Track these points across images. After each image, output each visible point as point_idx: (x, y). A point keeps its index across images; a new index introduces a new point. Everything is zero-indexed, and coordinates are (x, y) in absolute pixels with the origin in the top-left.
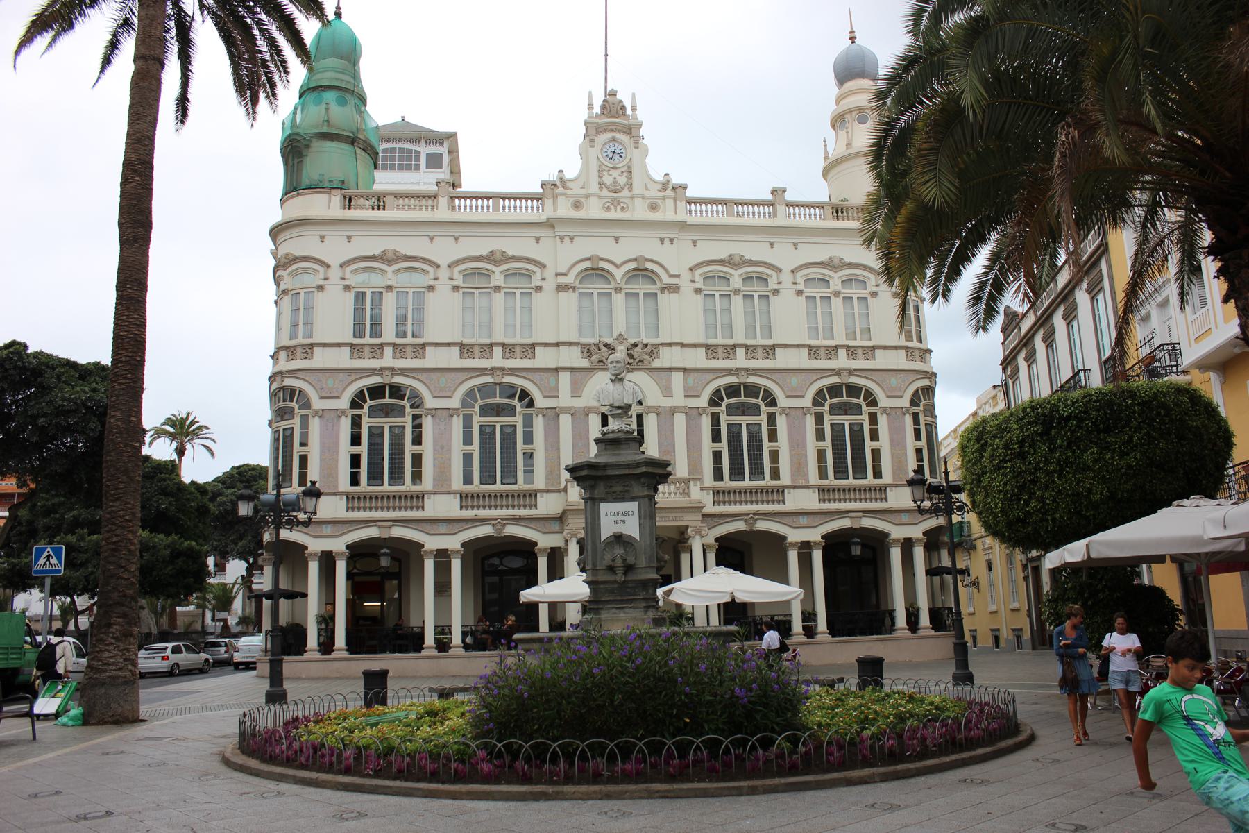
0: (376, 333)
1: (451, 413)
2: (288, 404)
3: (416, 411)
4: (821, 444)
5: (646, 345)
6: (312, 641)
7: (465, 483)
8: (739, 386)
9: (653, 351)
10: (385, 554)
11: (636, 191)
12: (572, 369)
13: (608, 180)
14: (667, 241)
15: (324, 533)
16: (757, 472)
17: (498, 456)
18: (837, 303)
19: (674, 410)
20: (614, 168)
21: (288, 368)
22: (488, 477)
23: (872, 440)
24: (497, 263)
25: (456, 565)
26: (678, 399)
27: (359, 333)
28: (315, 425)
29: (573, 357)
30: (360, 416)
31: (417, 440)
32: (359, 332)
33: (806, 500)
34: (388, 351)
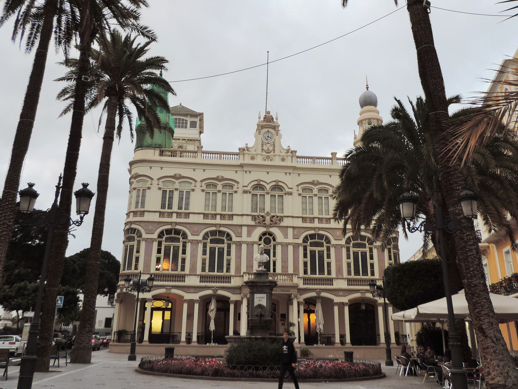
0: (170, 207)
1: (198, 242)
2: (132, 235)
3: (185, 240)
5: (278, 217)
11: (277, 152)
13: (265, 148)
17: (216, 260)
20: (268, 143)
22: (212, 269)
24: (220, 181)
26: (290, 240)
29: (248, 221)
30: (161, 242)
32: (163, 206)
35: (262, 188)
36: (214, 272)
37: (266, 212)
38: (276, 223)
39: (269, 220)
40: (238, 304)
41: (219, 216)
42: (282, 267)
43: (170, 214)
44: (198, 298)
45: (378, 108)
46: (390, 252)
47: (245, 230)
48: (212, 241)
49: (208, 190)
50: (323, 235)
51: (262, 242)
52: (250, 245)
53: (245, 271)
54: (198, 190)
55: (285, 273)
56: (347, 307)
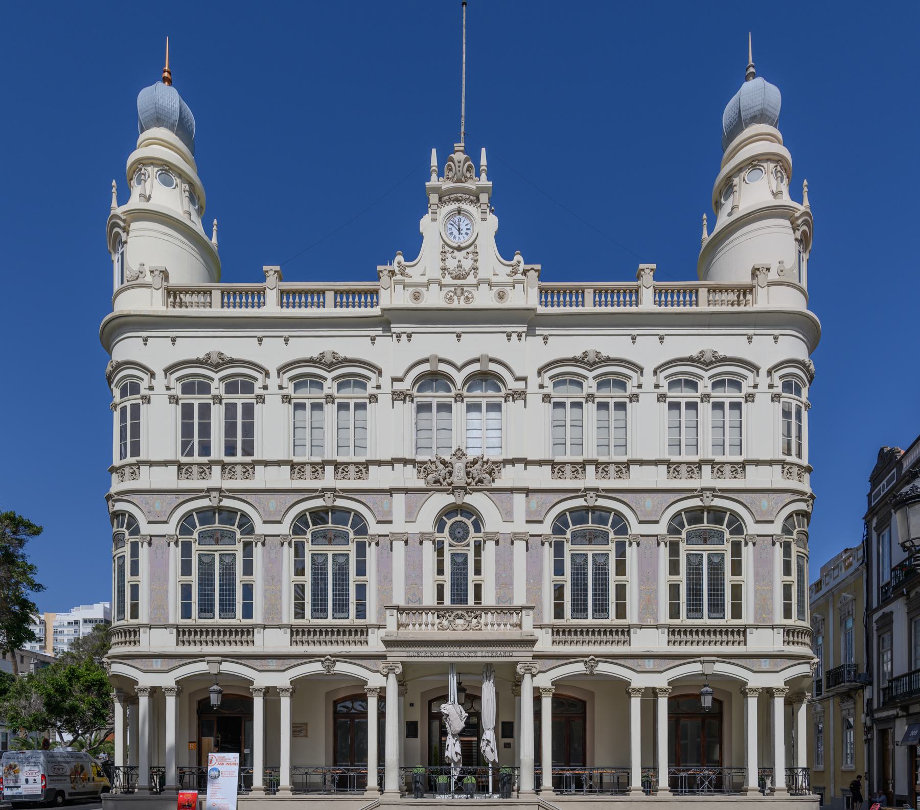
0: (205, 449)
1: (282, 540)
3: (248, 538)
4: (440, 577)
7: (671, 617)
9: (494, 467)
11: (482, 275)
12: (407, 491)
13: (451, 264)
15: (155, 668)
18: (705, 409)
19: (514, 538)
20: (459, 249)
24: (330, 366)
26: (519, 525)
27: (187, 449)
28: (489, 549)
29: (409, 477)
30: (303, 544)
31: (361, 571)
33: (274, 641)
34: (216, 470)
36: (326, 618)
38: (480, 481)
39: (463, 474)
41: (219, 468)
43: (205, 469)
44: (664, 685)
46: (440, 551)
56: (261, 699)
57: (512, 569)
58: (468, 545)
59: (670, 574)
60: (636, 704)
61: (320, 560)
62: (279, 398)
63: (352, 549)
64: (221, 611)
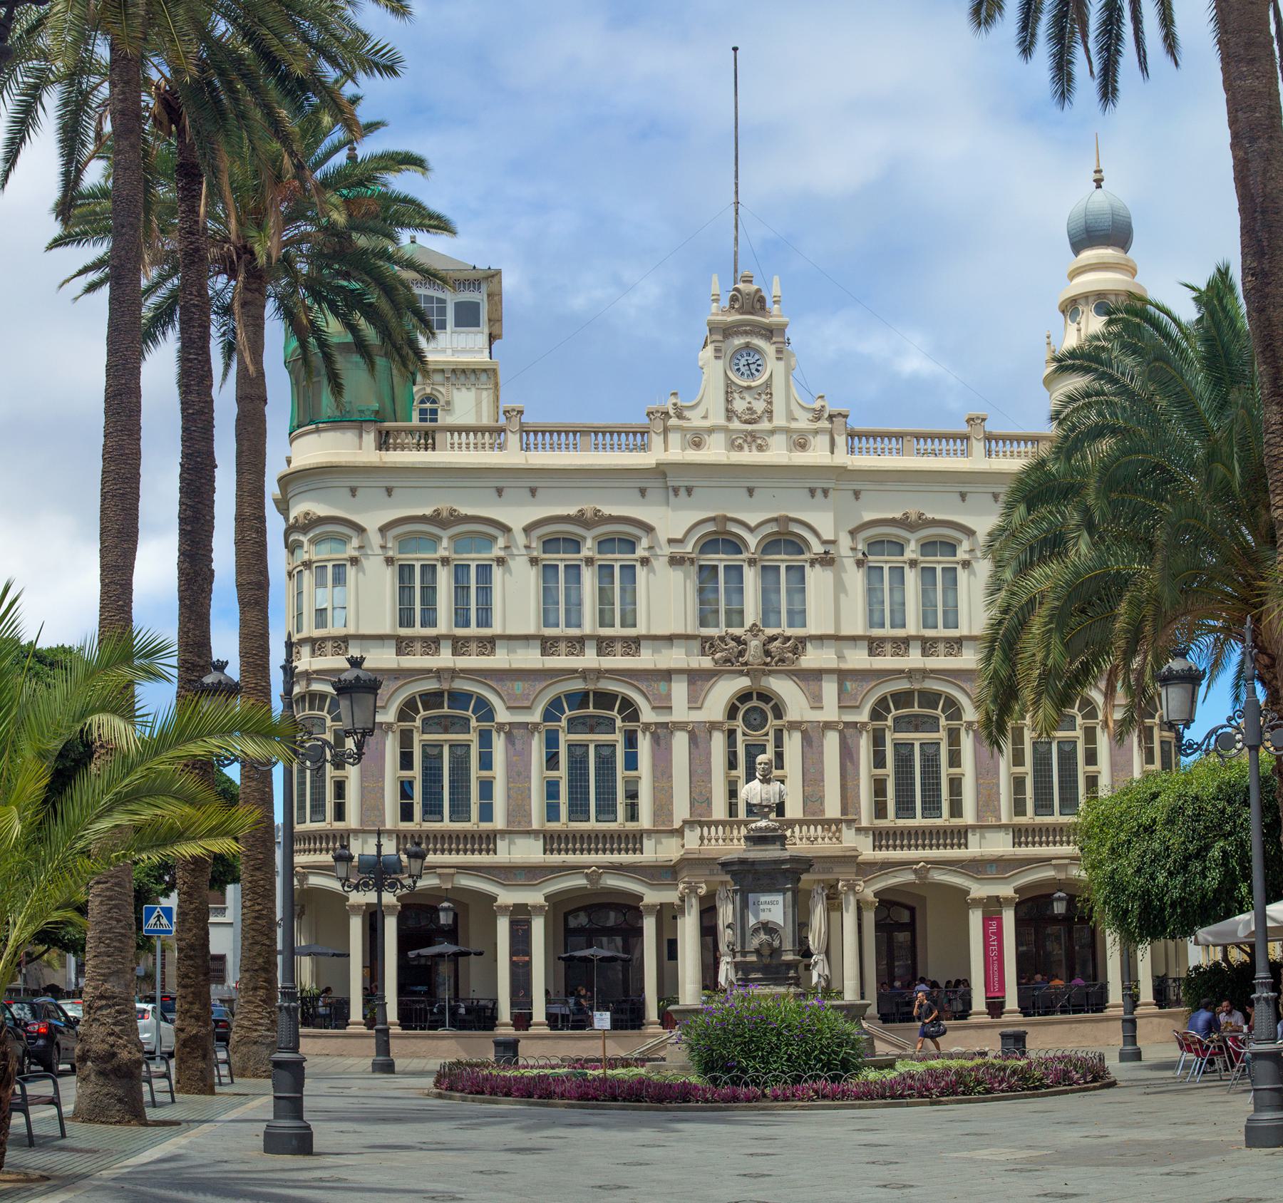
0: (429, 621)
4: (879, 771)
5: (789, 639)
6: (979, 1001)
8: (586, 694)
10: (1060, 899)
11: (780, 420)
13: (739, 405)
14: (819, 493)
16: (932, 807)
17: (590, 785)
19: (828, 726)
21: (315, 667)
23: (627, 768)
25: (538, 927)
26: (830, 712)
35: (735, 545)
37: (747, 626)
39: (760, 652)
40: (668, 916)
42: (806, 799)
45: (1134, 253)
47: (679, 690)
48: (574, 725)
49: (551, 558)
50: (938, 695)
51: (739, 724)
52: (698, 736)
53: (687, 816)
54: (520, 564)
55: (814, 818)
57: (822, 762)
58: (767, 734)
59: (402, 768)
60: (976, 919)
61: (579, 751)
62: (526, 559)
63: (618, 738)
64: (598, 812)
